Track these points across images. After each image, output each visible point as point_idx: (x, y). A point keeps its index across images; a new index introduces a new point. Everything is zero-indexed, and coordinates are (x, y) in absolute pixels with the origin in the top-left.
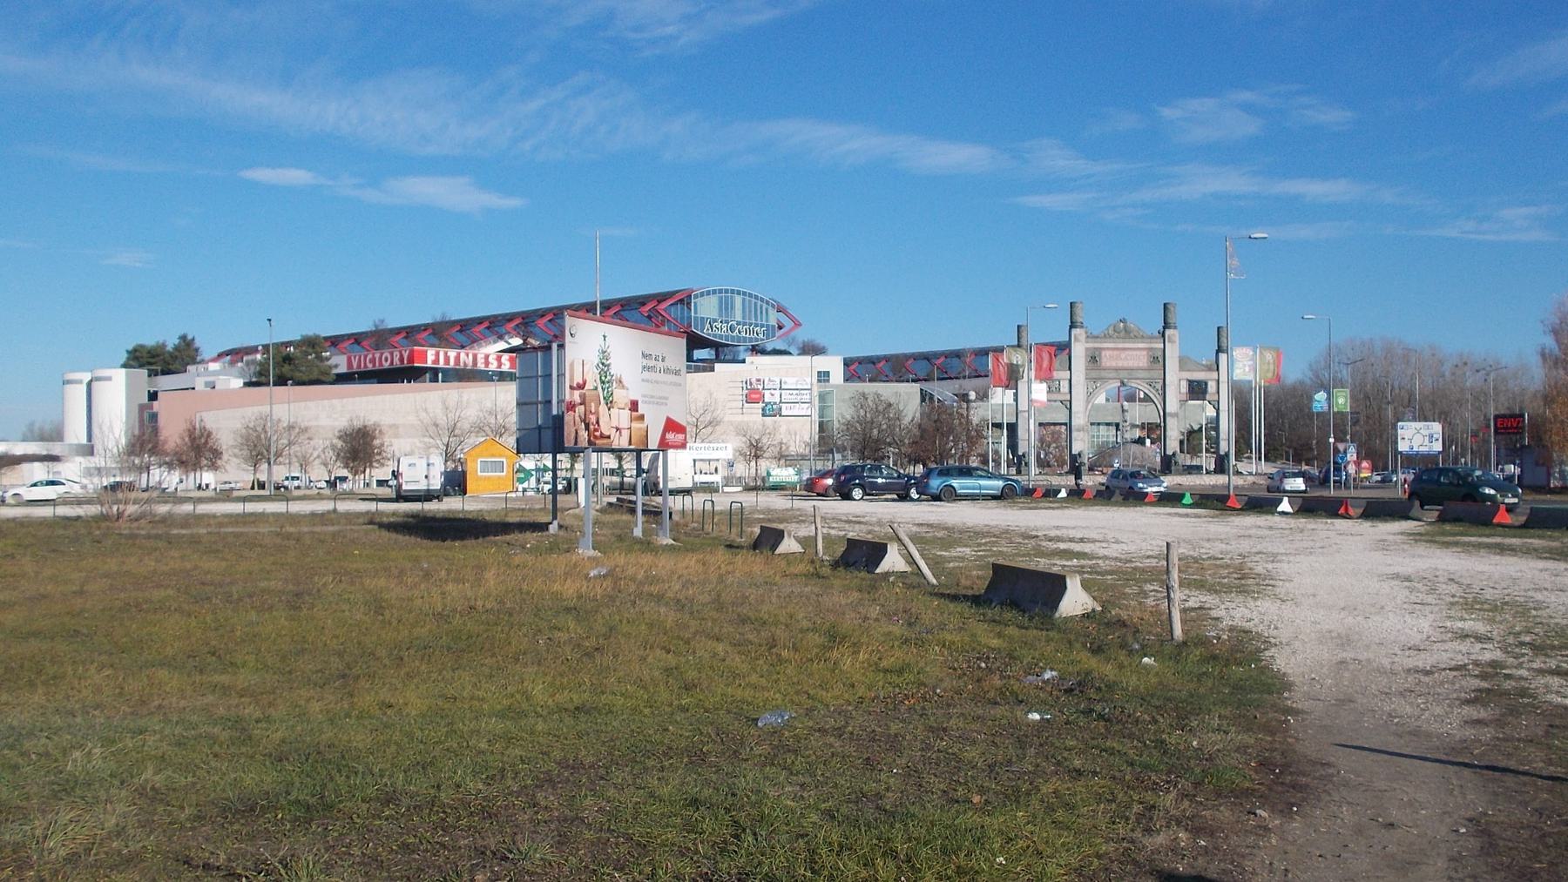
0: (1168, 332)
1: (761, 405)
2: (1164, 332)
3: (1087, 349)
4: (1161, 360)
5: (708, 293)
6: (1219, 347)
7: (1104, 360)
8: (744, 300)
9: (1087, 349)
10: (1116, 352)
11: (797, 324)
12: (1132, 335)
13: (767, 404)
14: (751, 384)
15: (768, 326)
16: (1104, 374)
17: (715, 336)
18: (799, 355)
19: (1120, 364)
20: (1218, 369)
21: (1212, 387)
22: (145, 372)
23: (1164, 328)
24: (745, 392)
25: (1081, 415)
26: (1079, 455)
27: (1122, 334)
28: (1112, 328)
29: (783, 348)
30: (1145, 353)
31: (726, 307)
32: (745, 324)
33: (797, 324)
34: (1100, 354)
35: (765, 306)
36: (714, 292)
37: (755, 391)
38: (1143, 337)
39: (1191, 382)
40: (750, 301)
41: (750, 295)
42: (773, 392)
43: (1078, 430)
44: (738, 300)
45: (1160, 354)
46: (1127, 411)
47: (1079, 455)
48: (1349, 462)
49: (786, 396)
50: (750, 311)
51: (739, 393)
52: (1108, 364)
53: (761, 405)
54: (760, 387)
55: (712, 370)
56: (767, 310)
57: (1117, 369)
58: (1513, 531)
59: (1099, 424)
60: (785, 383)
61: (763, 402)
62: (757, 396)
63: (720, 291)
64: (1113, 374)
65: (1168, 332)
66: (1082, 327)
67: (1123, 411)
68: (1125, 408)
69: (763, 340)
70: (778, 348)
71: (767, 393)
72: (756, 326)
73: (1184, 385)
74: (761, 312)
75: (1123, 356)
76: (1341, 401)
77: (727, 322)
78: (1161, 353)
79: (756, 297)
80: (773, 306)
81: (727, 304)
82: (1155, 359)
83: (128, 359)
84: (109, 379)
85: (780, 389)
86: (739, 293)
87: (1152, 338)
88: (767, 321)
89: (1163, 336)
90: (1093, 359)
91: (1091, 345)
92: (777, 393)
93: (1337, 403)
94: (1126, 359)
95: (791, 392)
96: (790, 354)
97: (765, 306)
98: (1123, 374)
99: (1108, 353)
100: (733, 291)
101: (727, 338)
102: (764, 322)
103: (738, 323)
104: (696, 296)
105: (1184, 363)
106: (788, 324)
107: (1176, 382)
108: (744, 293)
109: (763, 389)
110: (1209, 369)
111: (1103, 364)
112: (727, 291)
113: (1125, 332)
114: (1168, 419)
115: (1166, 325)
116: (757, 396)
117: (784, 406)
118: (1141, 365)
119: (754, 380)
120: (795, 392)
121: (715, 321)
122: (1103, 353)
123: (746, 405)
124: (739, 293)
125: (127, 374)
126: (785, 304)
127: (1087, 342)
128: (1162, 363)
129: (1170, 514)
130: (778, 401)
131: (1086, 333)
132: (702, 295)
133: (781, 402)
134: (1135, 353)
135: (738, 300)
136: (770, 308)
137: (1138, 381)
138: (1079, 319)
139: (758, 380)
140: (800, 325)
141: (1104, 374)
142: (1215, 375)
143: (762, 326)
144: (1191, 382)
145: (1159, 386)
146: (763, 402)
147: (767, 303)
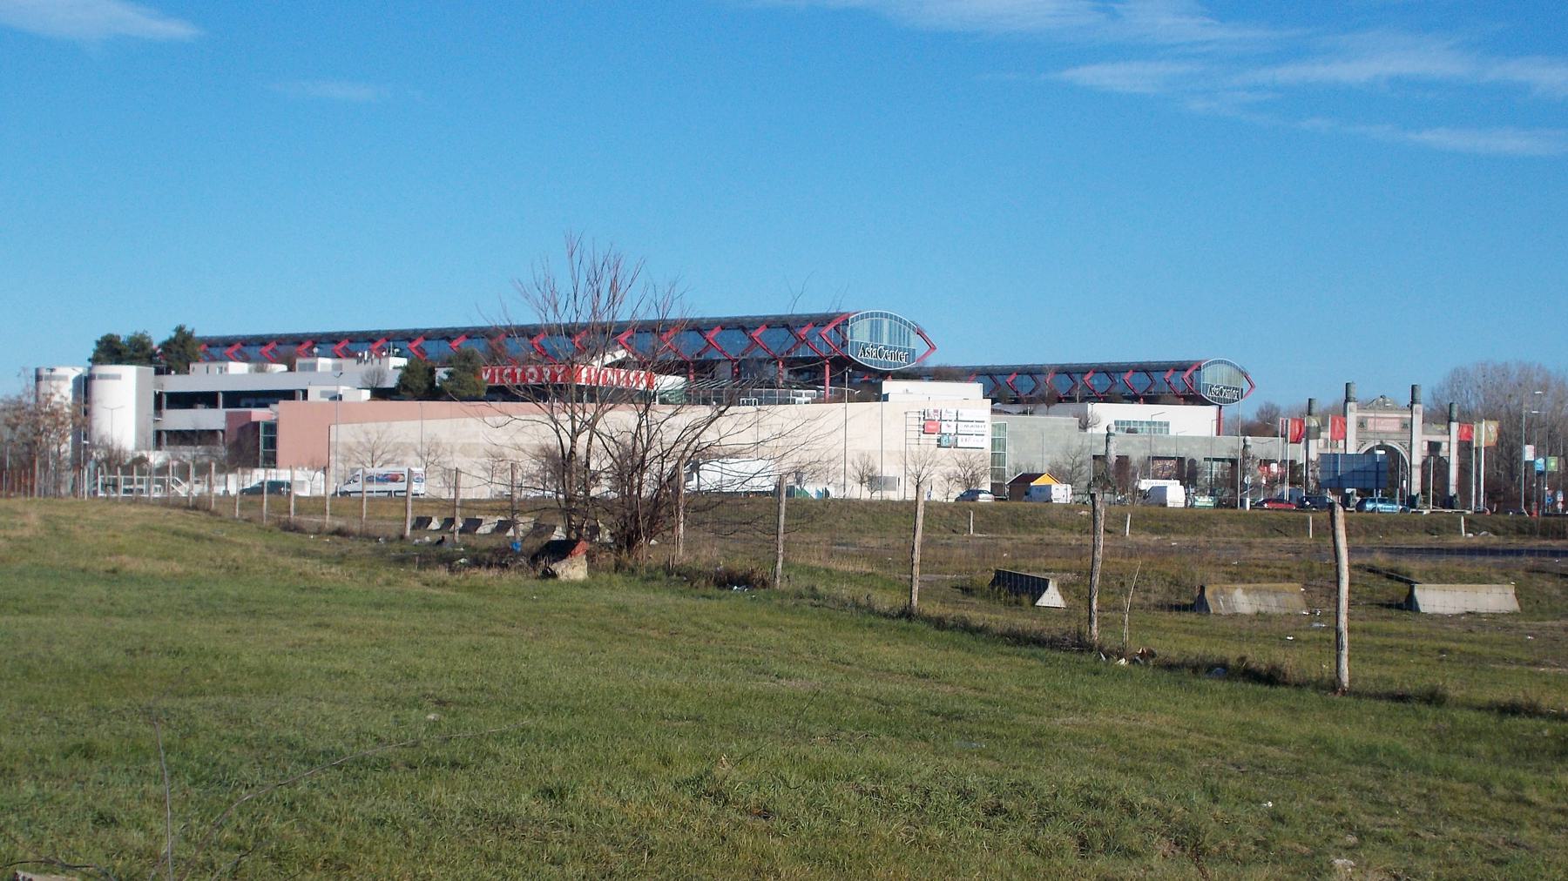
0: (1415, 406)
1: (936, 436)
17: (866, 361)
21: (1444, 446)
22: (152, 370)
23: (1412, 403)
24: (922, 423)
30: (1397, 420)
31: (875, 330)
39: (1430, 443)
40: (900, 327)
44: (886, 322)
45: (1408, 422)
49: (962, 428)
50: (900, 335)
51: (915, 423)
53: (936, 436)
58: (1465, 565)
68: (1248, 443)
73: (1426, 444)
76: (1553, 464)
81: (876, 327)
82: (1405, 426)
83: (96, 352)
84: (118, 377)
85: (957, 420)
86: (886, 315)
89: (1411, 408)
90: (1361, 424)
91: (1359, 414)
92: (953, 424)
94: (1384, 425)
98: (1382, 436)
100: (882, 315)
108: (891, 316)
110: (1443, 433)
113: (1381, 404)
115: (1413, 401)
119: (931, 411)
120: (970, 424)
121: (867, 345)
123: (922, 435)
125: (139, 373)
138: (1352, 395)
139: (935, 411)
142: (1447, 438)
144: (1430, 443)
145: (1407, 445)
147: (910, 326)
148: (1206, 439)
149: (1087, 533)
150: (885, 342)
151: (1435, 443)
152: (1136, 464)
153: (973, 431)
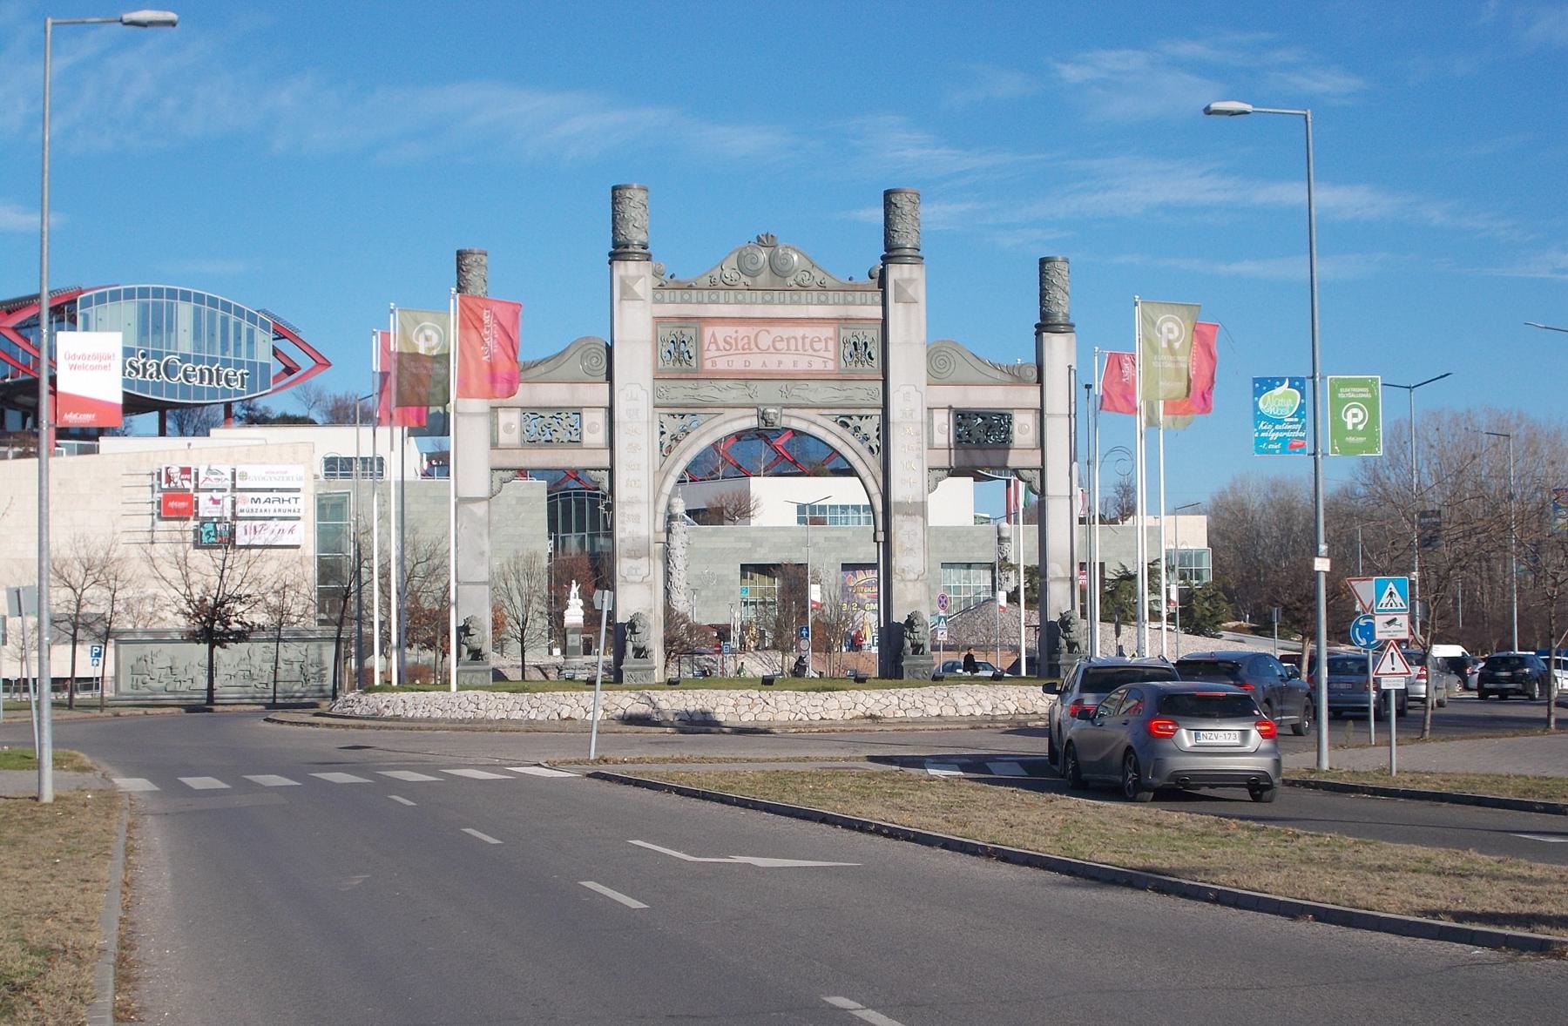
0: (895, 273)
2: (883, 275)
3: (659, 320)
4: (876, 351)
5: (115, 296)
6: (1044, 315)
7: (710, 353)
8: (197, 313)
9: (659, 320)
10: (743, 331)
11: (323, 363)
12: (790, 281)
13: (204, 521)
14: (169, 479)
15: (252, 366)
16: (707, 391)
18: (325, 425)
19: (756, 363)
20: (1040, 380)
21: (1023, 429)
23: (886, 260)
25: (644, 511)
26: (632, 625)
27: (763, 279)
28: (732, 262)
29: (299, 413)
30: (828, 331)
32: (198, 360)
33: (323, 363)
34: (699, 334)
35: (245, 325)
36: (129, 294)
37: (183, 494)
38: (823, 288)
39: (962, 417)
41: (213, 302)
42: (217, 495)
43: (634, 555)
44: (185, 311)
46: (1008, 539)
47: (632, 625)
48: (1381, 647)
49: (245, 506)
51: (146, 498)
52: (722, 365)
54: (189, 486)
55: (93, 450)
56: (251, 333)
57: (746, 378)
59: (969, 566)
60: (244, 476)
61: (197, 517)
62: (183, 504)
63: (144, 293)
64: (734, 394)
65: (895, 273)
66: (648, 258)
67: (1000, 539)
69: (242, 393)
70: (290, 412)
71: (203, 498)
72: (226, 363)
73: (942, 420)
74: (238, 337)
75: (765, 340)
77: (158, 355)
78: (873, 334)
79: (226, 307)
80: (264, 325)
82: (858, 349)
87: (850, 288)
88: (251, 354)
93: (1339, 425)
95: (256, 495)
96: (312, 423)
97: (245, 325)
98: (767, 394)
99: (721, 332)
100: (172, 294)
101: (158, 388)
102: (244, 358)
103: (185, 358)
104: (87, 303)
105: (939, 365)
106: (305, 363)
107: (920, 415)
108: (199, 299)
109: (197, 489)
110: (1015, 377)
111: (708, 365)
112: (158, 293)
114: (896, 520)
115: (892, 254)
116: (183, 504)
117: (240, 526)
118: (818, 365)
119: (175, 471)
120: (263, 496)
122: (708, 332)
124: (186, 296)
126: (291, 319)
127: (656, 301)
128: (877, 363)
129: (970, 779)
130: (228, 514)
131: (656, 274)
132: (101, 299)
133: (235, 517)
134: (799, 331)
135: (185, 311)
136: (258, 329)
137: (811, 414)
139: (186, 471)
140: (329, 365)
141: (707, 391)
142: (1031, 395)
143: (239, 365)
144: (962, 417)
145: (870, 427)
146: (197, 517)
148: (103, 435)
149: (33, 768)
150: (185, 344)
151: (984, 414)
152: (67, 553)
153: (272, 509)
